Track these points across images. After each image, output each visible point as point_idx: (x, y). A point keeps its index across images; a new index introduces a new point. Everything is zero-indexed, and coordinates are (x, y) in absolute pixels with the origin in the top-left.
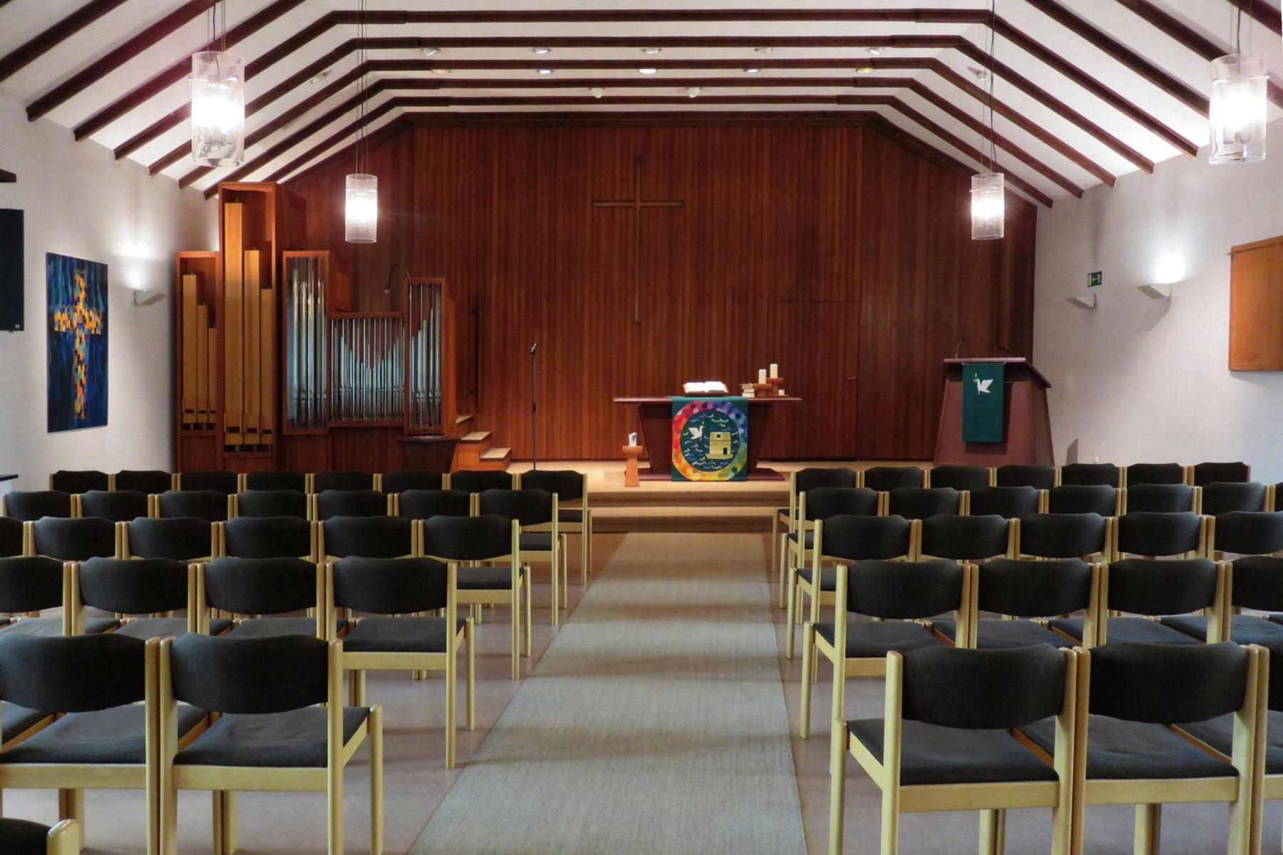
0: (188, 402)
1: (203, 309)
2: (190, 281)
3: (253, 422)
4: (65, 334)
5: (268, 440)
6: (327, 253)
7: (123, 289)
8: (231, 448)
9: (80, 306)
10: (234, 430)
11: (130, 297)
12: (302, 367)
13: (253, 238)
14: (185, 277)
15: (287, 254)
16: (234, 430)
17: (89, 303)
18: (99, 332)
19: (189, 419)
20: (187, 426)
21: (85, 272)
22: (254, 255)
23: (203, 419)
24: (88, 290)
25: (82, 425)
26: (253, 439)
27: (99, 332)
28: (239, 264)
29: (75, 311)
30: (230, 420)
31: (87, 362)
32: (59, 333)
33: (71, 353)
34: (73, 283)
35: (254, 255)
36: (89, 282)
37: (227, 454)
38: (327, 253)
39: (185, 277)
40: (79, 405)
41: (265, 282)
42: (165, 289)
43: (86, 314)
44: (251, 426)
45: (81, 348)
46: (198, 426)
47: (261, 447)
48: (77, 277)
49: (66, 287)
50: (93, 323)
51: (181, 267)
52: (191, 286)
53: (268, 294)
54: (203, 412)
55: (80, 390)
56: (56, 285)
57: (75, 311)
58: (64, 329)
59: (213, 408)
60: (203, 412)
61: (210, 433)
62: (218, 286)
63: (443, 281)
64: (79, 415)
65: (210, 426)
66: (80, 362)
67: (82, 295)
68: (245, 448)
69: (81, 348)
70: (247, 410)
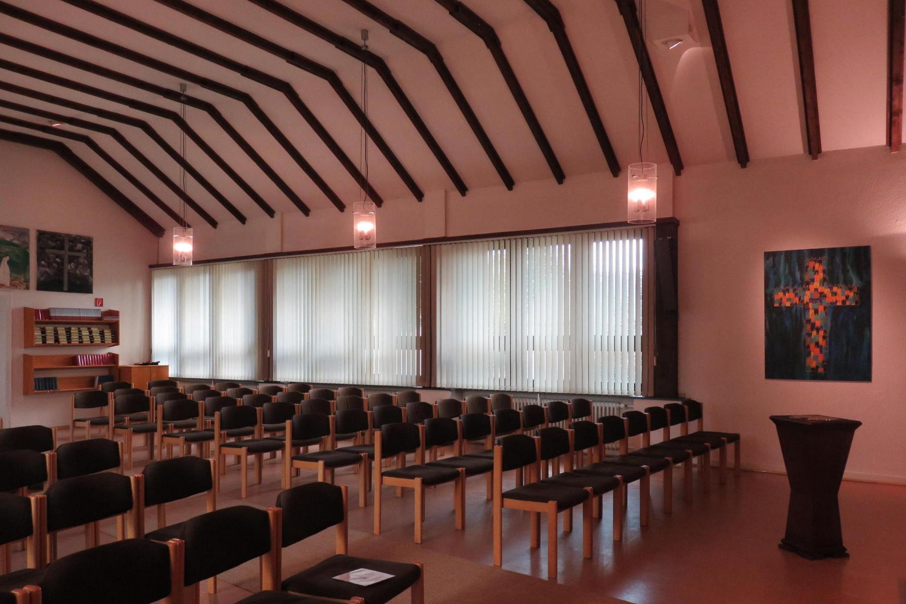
25: (815, 376)
58: (788, 304)
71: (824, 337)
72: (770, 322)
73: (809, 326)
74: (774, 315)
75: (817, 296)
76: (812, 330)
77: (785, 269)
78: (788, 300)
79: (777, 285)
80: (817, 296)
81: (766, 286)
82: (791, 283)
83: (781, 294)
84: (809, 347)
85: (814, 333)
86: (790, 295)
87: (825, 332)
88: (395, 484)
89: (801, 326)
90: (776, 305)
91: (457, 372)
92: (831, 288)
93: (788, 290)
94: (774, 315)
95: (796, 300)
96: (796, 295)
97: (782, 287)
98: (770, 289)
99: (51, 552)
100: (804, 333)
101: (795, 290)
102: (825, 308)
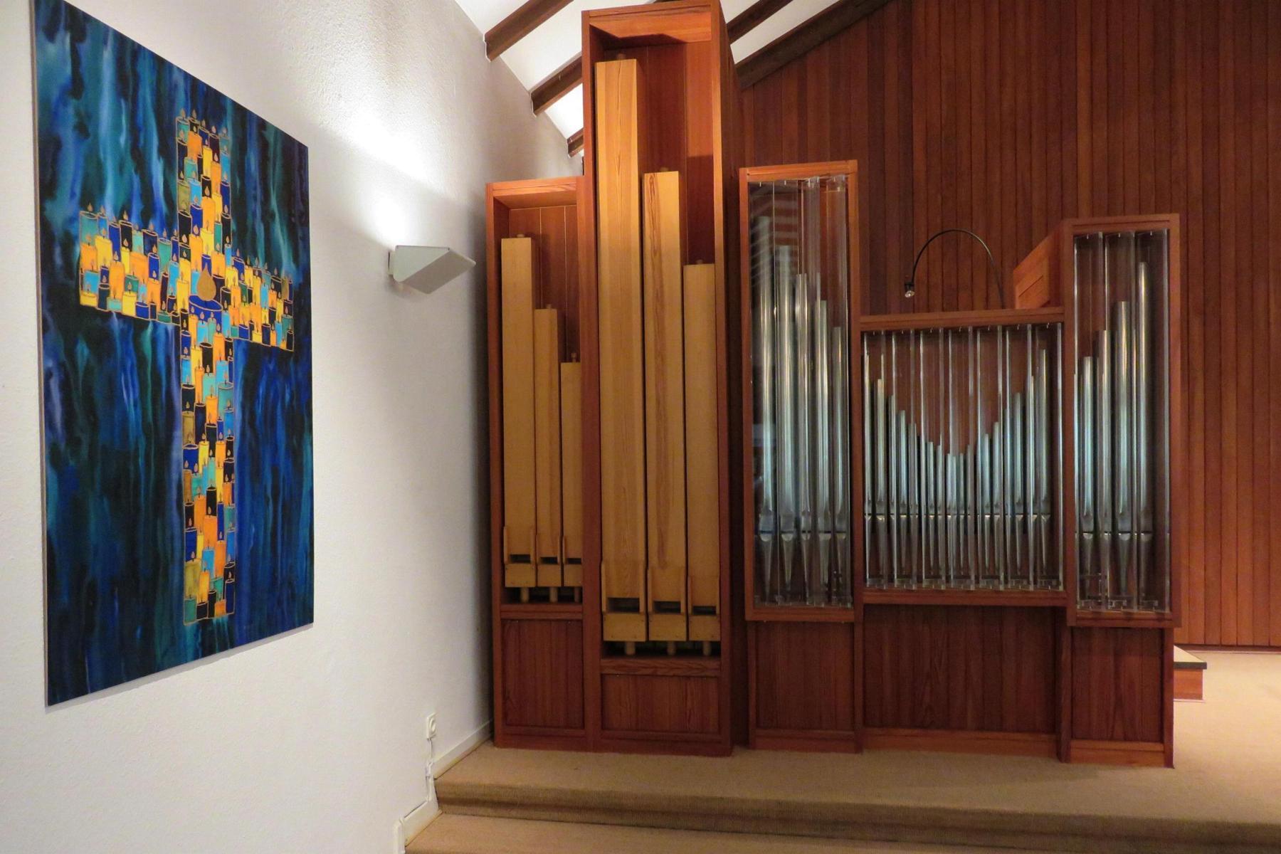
0: (517, 537)
1: (548, 317)
2: (517, 252)
3: (669, 588)
4: (135, 325)
5: (706, 630)
6: (844, 172)
7: (354, 237)
8: (614, 649)
9: (205, 241)
10: (625, 605)
11: (377, 269)
12: (795, 459)
13: (661, 144)
14: (506, 243)
15: (749, 175)
16: (625, 605)
17: (241, 237)
18: (278, 341)
19: (520, 577)
20: (513, 595)
21: (226, 135)
22: (668, 184)
23: (550, 578)
24: (236, 198)
25: (213, 641)
26: (670, 630)
27: (278, 341)
28: (637, 208)
29: (181, 252)
30: (613, 586)
31: (233, 430)
32: (101, 315)
33: (166, 398)
34: (173, 154)
35: (668, 184)
36: (239, 168)
37: (609, 664)
38: (844, 172)
39: (506, 243)
40: (202, 579)
41: (695, 246)
42: (460, 245)
43: (230, 275)
44: (666, 595)
45: (211, 387)
46: (539, 595)
47: (689, 650)
48: (191, 139)
49: (138, 155)
50: (257, 308)
51: (502, 218)
52: (521, 265)
53: (703, 277)
54: (550, 561)
55: (205, 526)
56: (85, 128)
57: (181, 252)
58: (128, 307)
59: (575, 550)
60: (550, 561)
61: (568, 612)
62: (583, 256)
63: (1170, 224)
64: (205, 610)
65: (566, 595)
66: (206, 432)
67: (214, 208)
68: (650, 649)
69: (211, 387)
70: (654, 560)
71: (228, 469)
72: (65, 387)
73: (188, 422)
74: (83, 351)
75: (209, 295)
76: (198, 440)
77: (117, 127)
78: (130, 283)
79: (90, 197)
80: (209, 295)
81: (47, 187)
82: (137, 207)
83: (103, 246)
84: (190, 512)
85: (204, 449)
86: (133, 261)
87: (229, 446)
88: (532, 607)
89: (171, 421)
90: (89, 299)
91: (754, 250)
92: (241, 270)
93: (127, 233)
94: (83, 351)
95: (151, 292)
96: (154, 265)
97: (108, 211)
98: (63, 208)
99: (844, 464)
100: (177, 453)
101: (150, 242)
102: (228, 346)
